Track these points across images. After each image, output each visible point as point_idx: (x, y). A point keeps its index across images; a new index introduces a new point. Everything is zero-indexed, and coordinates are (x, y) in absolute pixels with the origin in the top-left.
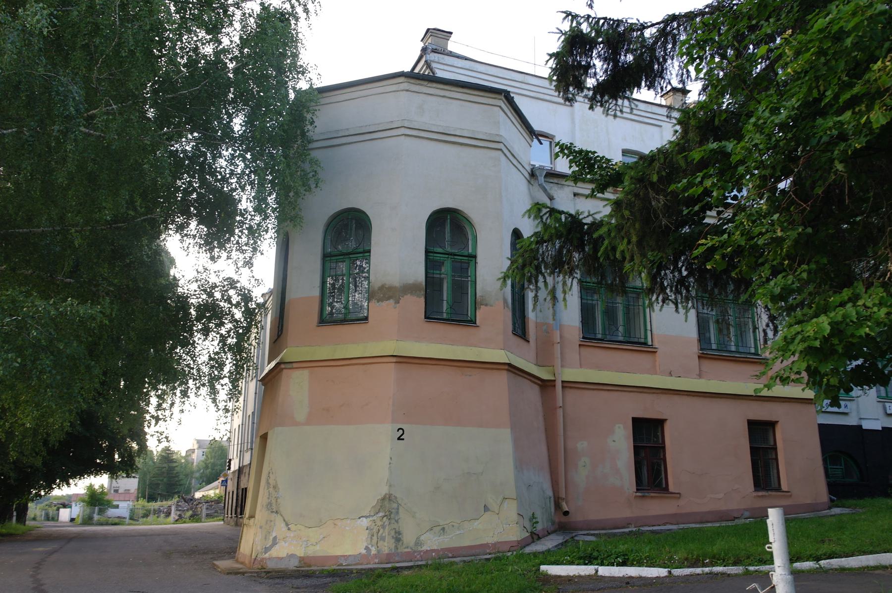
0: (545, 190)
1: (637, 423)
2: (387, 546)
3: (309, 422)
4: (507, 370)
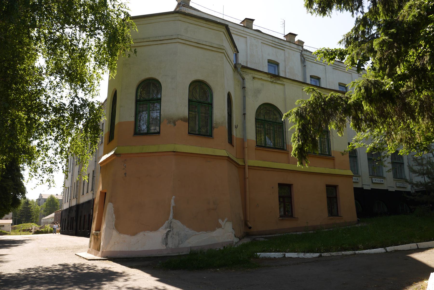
0: (241, 75)
1: (281, 186)
2: (164, 247)
4: (227, 160)
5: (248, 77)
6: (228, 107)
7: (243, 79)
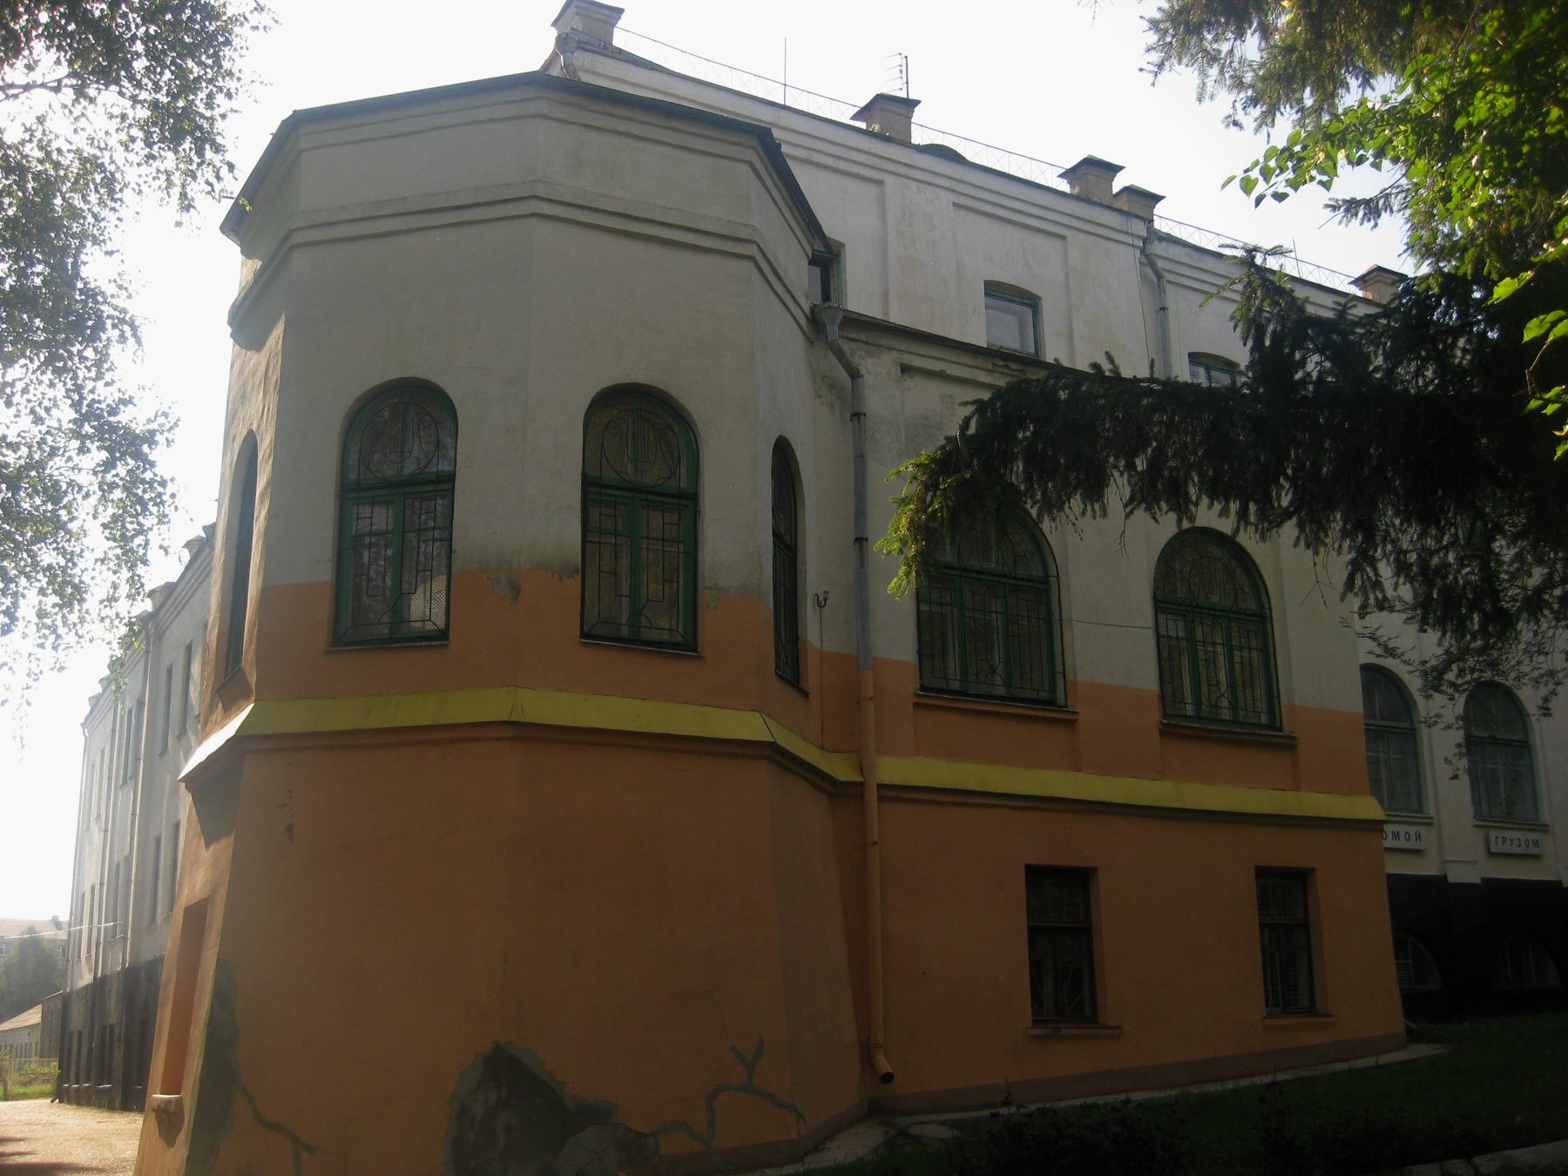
0: (840, 356)
1: (1036, 875)
5: (878, 368)
6: (776, 509)
7: (855, 374)
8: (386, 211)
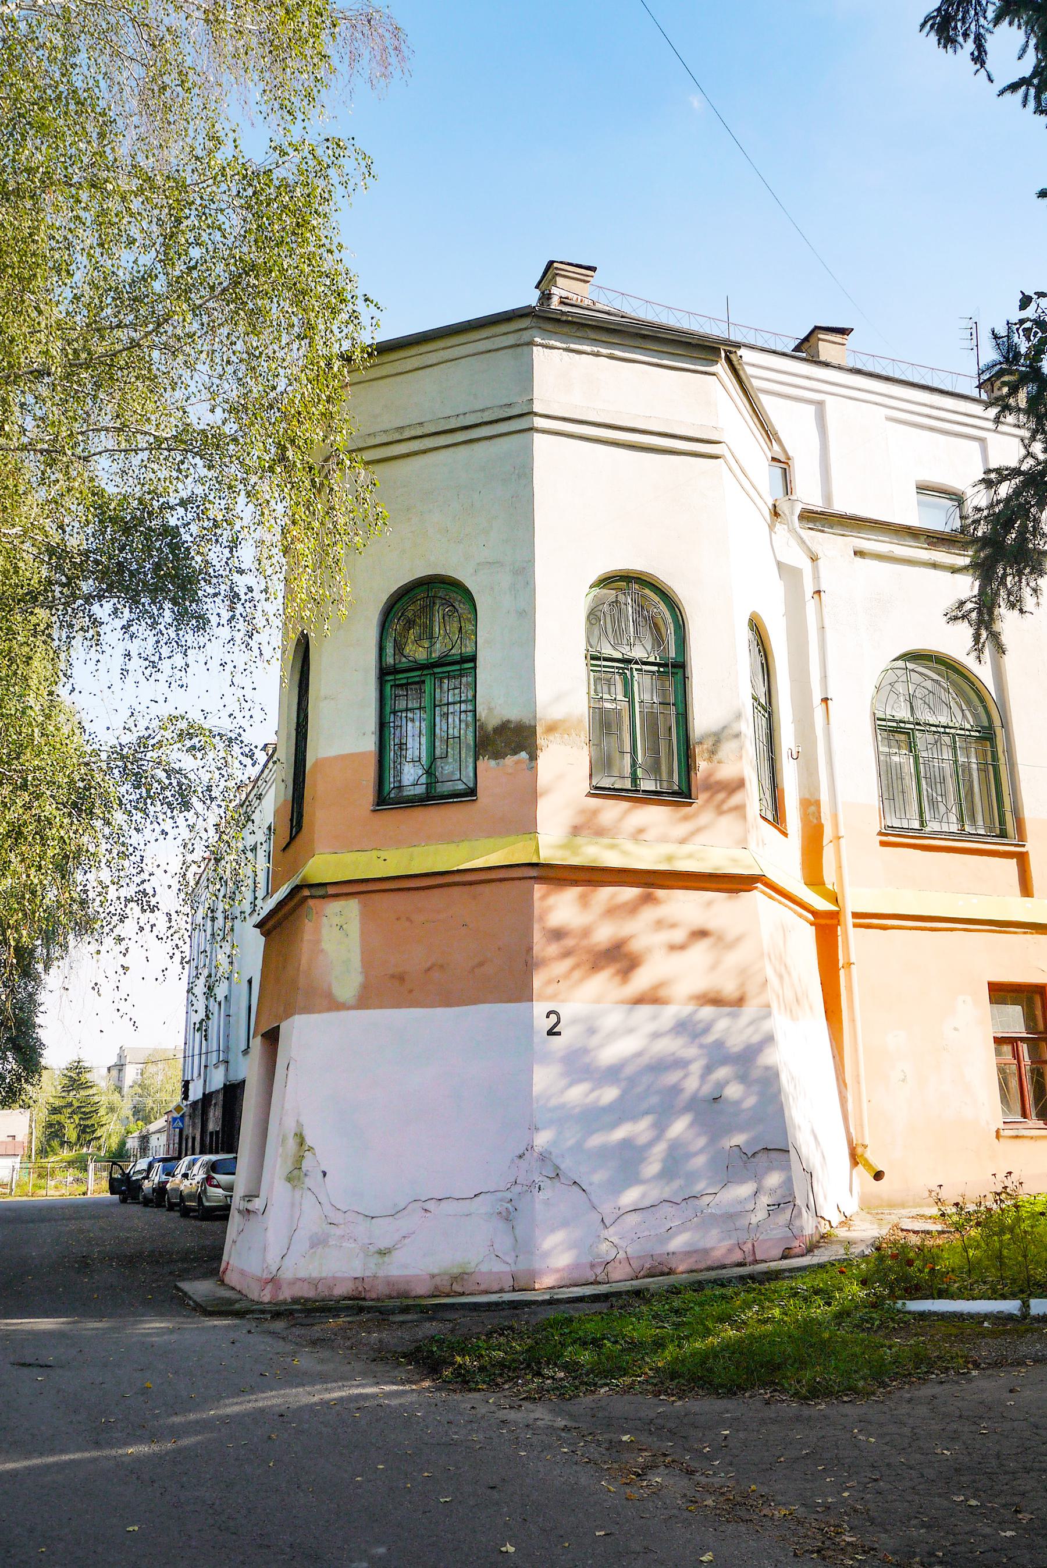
3: (366, 1000)
8: (407, 434)
